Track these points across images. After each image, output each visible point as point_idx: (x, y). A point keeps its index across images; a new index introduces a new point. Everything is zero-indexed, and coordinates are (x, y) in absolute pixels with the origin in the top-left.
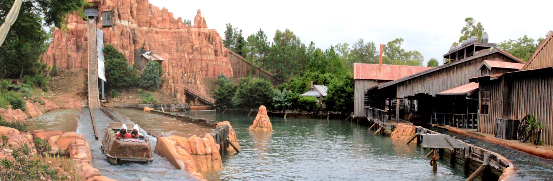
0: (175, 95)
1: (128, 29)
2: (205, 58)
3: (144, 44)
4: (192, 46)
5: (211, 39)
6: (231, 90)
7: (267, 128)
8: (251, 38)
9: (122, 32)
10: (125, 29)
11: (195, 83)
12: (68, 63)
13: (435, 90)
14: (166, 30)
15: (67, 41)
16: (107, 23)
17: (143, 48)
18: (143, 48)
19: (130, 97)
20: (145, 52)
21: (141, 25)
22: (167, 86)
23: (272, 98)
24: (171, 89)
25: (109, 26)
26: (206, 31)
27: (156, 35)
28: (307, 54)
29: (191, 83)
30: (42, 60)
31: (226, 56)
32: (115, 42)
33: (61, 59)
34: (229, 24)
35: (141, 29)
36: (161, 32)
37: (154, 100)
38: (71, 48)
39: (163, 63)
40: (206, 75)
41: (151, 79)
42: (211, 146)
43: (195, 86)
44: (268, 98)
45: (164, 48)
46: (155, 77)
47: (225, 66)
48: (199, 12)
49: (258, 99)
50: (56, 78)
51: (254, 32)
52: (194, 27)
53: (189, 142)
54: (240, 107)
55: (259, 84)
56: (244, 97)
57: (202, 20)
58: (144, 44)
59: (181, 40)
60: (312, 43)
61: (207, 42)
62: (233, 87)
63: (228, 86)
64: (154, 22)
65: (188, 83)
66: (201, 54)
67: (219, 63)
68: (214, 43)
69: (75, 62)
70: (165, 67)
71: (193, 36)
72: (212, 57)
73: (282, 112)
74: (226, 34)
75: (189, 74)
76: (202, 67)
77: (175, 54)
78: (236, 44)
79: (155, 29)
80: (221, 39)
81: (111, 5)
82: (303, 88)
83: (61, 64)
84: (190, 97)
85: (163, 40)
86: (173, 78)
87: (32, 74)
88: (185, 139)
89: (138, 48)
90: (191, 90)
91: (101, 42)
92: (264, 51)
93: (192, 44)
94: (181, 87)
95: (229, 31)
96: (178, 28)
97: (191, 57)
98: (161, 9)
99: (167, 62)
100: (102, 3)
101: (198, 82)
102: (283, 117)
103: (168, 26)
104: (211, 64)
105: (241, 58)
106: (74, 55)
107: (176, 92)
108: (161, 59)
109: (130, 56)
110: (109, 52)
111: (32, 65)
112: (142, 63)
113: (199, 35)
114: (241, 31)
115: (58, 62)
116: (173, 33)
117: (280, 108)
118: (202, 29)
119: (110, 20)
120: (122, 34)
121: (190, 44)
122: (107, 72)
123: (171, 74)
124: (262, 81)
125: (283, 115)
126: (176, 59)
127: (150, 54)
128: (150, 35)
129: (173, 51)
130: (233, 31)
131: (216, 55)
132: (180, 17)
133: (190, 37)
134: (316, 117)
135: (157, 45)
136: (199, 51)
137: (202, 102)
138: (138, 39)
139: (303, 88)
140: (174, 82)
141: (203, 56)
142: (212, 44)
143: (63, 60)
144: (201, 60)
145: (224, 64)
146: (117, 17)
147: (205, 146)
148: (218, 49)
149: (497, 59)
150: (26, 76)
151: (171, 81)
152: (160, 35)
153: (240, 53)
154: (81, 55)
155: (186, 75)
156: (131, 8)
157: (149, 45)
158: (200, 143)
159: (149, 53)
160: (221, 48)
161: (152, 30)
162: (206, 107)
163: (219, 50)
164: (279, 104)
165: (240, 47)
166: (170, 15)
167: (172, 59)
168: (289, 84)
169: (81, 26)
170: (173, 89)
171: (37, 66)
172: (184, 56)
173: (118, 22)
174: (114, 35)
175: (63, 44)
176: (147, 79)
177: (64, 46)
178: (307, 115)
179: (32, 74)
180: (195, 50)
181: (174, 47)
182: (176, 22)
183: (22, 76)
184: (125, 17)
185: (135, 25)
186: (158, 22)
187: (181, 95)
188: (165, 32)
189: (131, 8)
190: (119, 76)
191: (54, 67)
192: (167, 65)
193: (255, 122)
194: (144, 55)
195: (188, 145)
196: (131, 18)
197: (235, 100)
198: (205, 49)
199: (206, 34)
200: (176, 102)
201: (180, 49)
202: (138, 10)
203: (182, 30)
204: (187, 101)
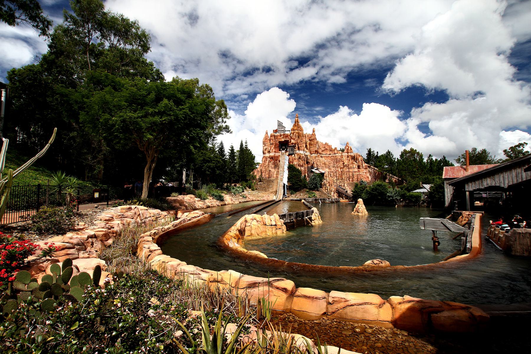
2: (351, 170)
4: (344, 164)
10: (302, 156)
13: (506, 182)
16: (291, 153)
26: (352, 154)
31: (366, 169)
40: (353, 181)
59: (337, 161)
64: (320, 151)
72: (356, 170)
83: (265, 175)
84: (340, 194)
86: (329, 182)
87: (247, 181)
91: (287, 163)
94: (333, 188)
101: (346, 185)
106: (273, 170)
108: (323, 172)
109: (305, 171)
110: (291, 168)
113: (348, 157)
115: (263, 174)
118: (349, 154)
120: (300, 158)
122: (289, 179)
127: (317, 170)
148: (360, 164)
149: (439, 90)
151: (327, 185)
156: (306, 143)
166: (330, 147)
169: (277, 154)
173: (298, 152)
175: (267, 164)
181: (332, 165)
185: (308, 153)
186: (323, 151)
195: (261, 219)
196: (305, 149)
202: (310, 144)
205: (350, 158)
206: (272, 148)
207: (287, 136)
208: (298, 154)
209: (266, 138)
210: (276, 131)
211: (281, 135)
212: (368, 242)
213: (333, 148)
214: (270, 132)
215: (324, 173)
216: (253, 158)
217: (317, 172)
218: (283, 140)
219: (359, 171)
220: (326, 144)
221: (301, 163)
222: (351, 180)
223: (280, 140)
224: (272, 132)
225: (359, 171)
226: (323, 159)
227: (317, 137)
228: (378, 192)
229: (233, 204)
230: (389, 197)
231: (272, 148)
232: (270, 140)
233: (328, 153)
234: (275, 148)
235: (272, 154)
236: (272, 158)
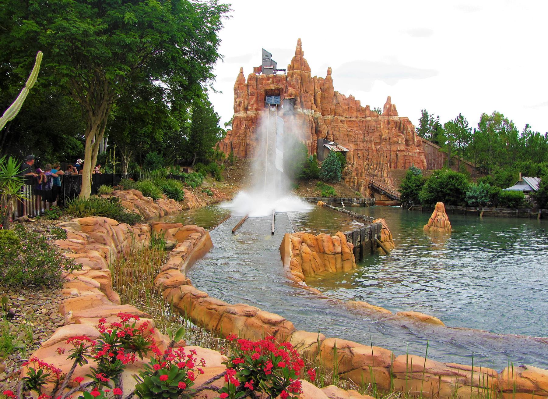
0: (358, 188)
2: (394, 148)
3: (328, 134)
4: (380, 136)
5: (402, 128)
6: (419, 183)
7: (444, 227)
8: (449, 124)
11: (382, 176)
14: (352, 119)
15: (246, 129)
17: (326, 138)
18: (326, 138)
20: (327, 142)
21: (325, 113)
22: (350, 179)
23: (465, 193)
24: (354, 182)
26: (397, 119)
27: (341, 124)
28: (520, 140)
29: (377, 176)
30: (218, 147)
31: (419, 145)
34: (425, 111)
35: (325, 118)
36: (347, 121)
37: (334, 193)
39: (348, 154)
40: (396, 167)
41: (332, 172)
42: (341, 245)
43: (382, 179)
44: (461, 193)
45: (348, 138)
46: (336, 169)
47: (418, 158)
48: (389, 99)
49: (448, 194)
50: (232, 167)
51: (451, 117)
52: (383, 115)
53: (317, 240)
54: (428, 203)
55: (451, 177)
56: (433, 192)
58: (328, 134)
59: (368, 129)
60: (527, 126)
61: (397, 131)
62: (421, 180)
63: (415, 180)
64: (340, 111)
65: (374, 176)
66: (390, 144)
67: (410, 154)
68: (405, 132)
70: (350, 158)
72: (403, 148)
73: (478, 209)
74: (421, 122)
76: (390, 159)
77: (362, 145)
78: (432, 132)
79: (340, 118)
80: (414, 128)
81: (294, 92)
82: (510, 181)
84: (374, 190)
87: (207, 163)
88: (312, 236)
89: (320, 138)
90: (377, 184)
92: (464, 139)
93: (380, 133)
95: (425, 116)
96: (366, 117)
97: (378, 147)
98: (347, 96)
99: (352, 153)
100: (284, 90)
101: (385, 175)
102: (479, 215)
103: (354, 115)
104: (400, 155)
105: (437, 147)
107: (359, 185)
108: (345, 150)
111: (206, 153)
112: (325, 155)
113: (388, 123)
114: (438, 117)
116: (360, 122)
117: (476, 205)
118: (391, 118)
121: (378, 134)
124: (454, 172)
125: (479, 213)
127: (334, 145)
128: (335, 124)
130: (429, 118)
131: (407, 145)
132: (368, 104)
134: (522, 216)
135: (342, 135)
136: (388, 141)
137: (389, 196)
138: (322, 129)
139: (509, 181)
140: (357, 175)
141: (392, 146)
142: (403, 133)
143: (241, 149)
144: (390, 150)
145: (416, 155)
147: (334, 245)
150: (199, 163)
151: (354, 174)
152: (346, 125)
153: (437, 143)
155: (372, 167)
156: (315, 96)
158: (328, 242)
159: (332, 143)
160: (413, 137)
161: (337, 119)
162: (392, 202)
164: (474, 200)
165: (436, 135)
166: (357, 103)
167: (358, 150)
168: (493, 176)
170: (356, 182)
171: (211, 154)
172: (371, 147)
175: (242, 131)
176: (327, 171)
178: (509, 213)
179: (207, 163)
180: (383, 140)
181: (360, 137)
182: (364, 111)
183: (195, 163)
185: (318, 114)
187: (366, 188)
188: (351, 121)
189: (315, 96)
191: (231, 156)
192: (352, 156)
193: (430, 220)
194: (326, 145)
195: (315, 242)
196: (314, 106)
197: (423, 194)
199: (396, 123)
200: (358, 196)
201: (367, 139)
202: (323, 98)
203: (369, 118)
204: (372, 195)
205: (392, 125)
206: (252, 102)
207: (278, 79)
210: (258, 70)
211: (268, 79)
214: (248, 72)
215: (345, 152)
216: (215, 119)
217: (335, 149)
222: (393, 165)
223: (267, 88)
225: (407, 150)
227: (334, 84)
229: (197, 207)
230: (471, 198)
231: (252, 102)
234: (257, 101)
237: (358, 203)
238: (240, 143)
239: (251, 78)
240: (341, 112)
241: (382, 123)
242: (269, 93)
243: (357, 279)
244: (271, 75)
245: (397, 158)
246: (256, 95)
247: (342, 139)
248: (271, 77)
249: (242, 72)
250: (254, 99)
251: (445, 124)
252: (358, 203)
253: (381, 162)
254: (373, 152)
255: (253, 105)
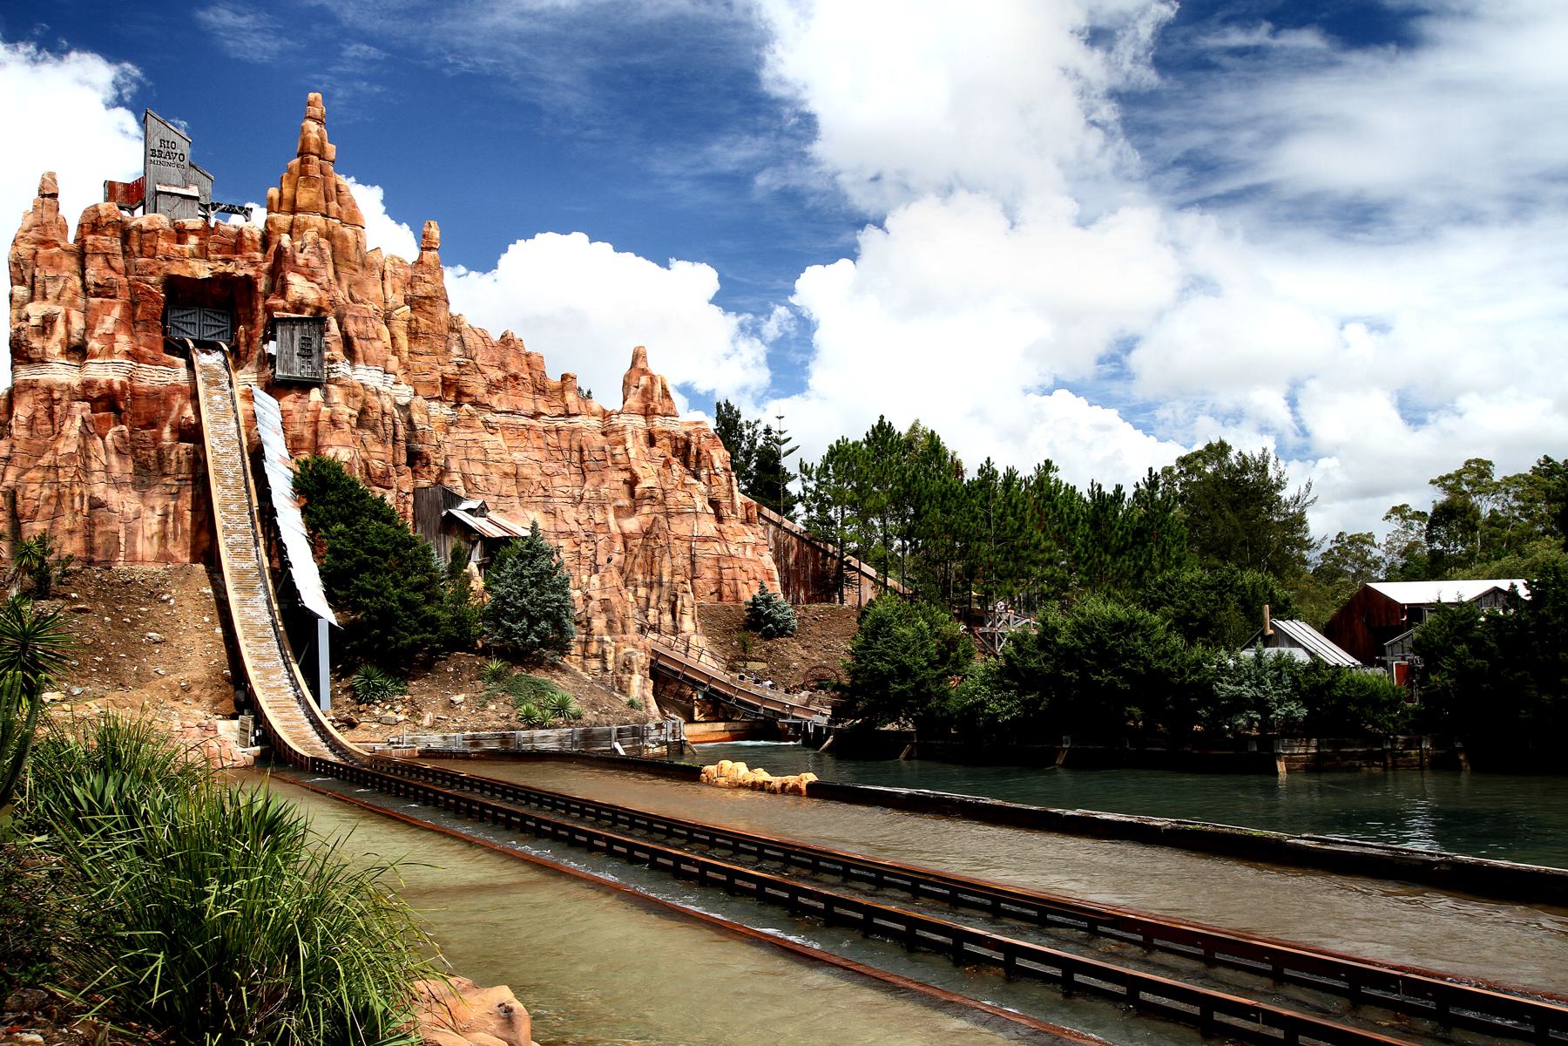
1: (388, 406)
4: (632, 482)
9: (363, 412)
11: (676, 630)
12: (89, 538)
15: (85, 434)
19: (459, 698)
25: (304, 386)
32: (340, 450)
33: (53, 518)
36: (505, 427)
38: (107, 469)
48: (1432, 482)
57: (658, 389)
68: (704, 473)
69: (131, 533)
71: (629, 445)
72: (708, 526)
75: (642, 592)
77: (570, 513)
85: (517, 456)
86: (606, 607)
93: (627, 475)
101: (688, 624)
106: (124, 502)
118: (658, 423)
119: (315, 360)
120: (363, 419)
123: (597, 595)
126: (571, 533)
129: (558, 502)
133: (619, 449)
135: (495, 478)
141: (675, 520)
142: (697, 477)
143: (66, 522)
145: (749, 553)
146: (337, 351)
148: (721, 493)
151: (599, 623)
154: (158, 503)
157: (465, 477)
159: (474, 504)
163: (725, 502)
169: (152, 377)
170: (610, 657)
172: (606, 524)
173: (343, 368)
174: (334, 422)
175: (67, 446)
176: (523, 612)
177: (71, 456)
180: (643, 497)
184: (372, 353)
186: (493, 387)
190: (401, 600)
198: (680, 496)
199: (673, 438)
206: (108, 324)
208: (351, 392)
209: (41, 232)
210: (132, 194)
212: (984, 1024)
213: (554, 378)
218: (202, 270)
219: (721, 537)
220: (506, 341)
221: (379, 456)
223: (177, 269)
224: (97, 197)
225: (721, 537)
226: (499, 438)
228: (1129, 676)
231: (108, 324)
232: (81, 255)
233: (528, 406)
235: (105, 372)
236: (108, 402)
237: (661, 744)
238: (60, 496)
239: (93, 224)
240: (482, 390)
241: (629, 438)
242: (181, 292)
243: (177, 973)
244: (195, 222)
245: (693, 563)
246: (123, 297)
247: (495, 490)
248: (193, 232)
249: (49, 195)
250: (117, 312)
251: (840, 455)
252: (661, 744)
253: (665, 579)
254: (611, 539)
255: (110, 337)
